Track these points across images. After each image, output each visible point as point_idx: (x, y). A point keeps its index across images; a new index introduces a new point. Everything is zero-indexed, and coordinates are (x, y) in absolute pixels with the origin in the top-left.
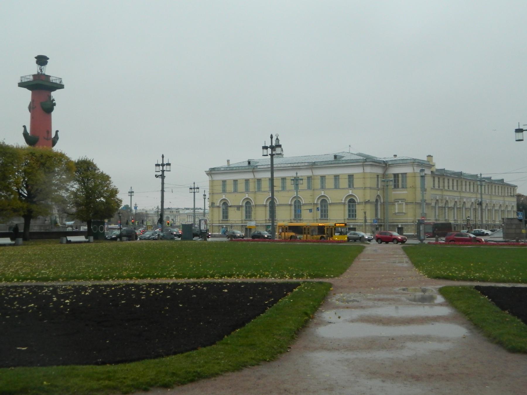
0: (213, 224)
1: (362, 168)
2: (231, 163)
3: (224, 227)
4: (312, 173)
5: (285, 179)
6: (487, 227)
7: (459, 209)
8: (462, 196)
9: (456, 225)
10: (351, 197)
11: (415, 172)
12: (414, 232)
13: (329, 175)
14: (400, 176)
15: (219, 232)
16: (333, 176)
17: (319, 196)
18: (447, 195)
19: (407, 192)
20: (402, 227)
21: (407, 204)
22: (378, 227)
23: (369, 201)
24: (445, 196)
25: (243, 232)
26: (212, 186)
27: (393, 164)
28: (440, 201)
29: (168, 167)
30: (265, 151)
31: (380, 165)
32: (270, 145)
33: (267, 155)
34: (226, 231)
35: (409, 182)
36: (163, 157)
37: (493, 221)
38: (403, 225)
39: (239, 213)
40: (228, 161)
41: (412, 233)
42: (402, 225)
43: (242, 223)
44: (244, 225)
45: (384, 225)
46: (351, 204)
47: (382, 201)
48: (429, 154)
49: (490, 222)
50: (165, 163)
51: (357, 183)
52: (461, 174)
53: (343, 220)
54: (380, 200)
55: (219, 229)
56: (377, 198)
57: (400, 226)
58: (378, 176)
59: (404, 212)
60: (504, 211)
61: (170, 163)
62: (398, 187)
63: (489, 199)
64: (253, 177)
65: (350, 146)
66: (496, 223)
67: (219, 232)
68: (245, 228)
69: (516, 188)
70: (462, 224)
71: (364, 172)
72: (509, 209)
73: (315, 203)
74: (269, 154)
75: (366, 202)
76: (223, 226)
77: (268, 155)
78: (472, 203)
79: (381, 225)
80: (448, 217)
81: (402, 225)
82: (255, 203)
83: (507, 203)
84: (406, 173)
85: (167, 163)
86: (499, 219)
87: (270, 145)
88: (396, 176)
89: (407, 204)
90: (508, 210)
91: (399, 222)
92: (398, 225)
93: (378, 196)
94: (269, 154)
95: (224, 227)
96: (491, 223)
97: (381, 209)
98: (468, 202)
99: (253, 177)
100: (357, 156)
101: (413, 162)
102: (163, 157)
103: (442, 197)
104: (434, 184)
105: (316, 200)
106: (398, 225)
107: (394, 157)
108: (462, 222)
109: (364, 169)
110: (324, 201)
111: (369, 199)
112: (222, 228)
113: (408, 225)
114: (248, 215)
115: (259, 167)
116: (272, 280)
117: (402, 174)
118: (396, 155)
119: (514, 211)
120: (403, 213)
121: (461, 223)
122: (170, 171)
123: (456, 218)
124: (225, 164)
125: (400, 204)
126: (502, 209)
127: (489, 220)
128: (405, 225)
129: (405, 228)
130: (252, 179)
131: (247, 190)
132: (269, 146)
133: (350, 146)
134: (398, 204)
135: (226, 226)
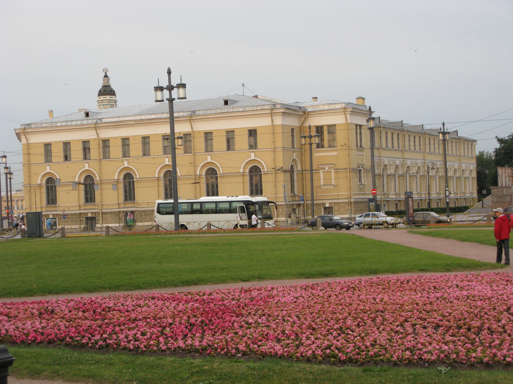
0: (102, 209)
1: (270, 118)
2: (55, 115)
3: (51, 217)
4: (192, 128)
5: (189, 136)
6: (399, 204)
7: (423, 178)
8: (405, 157)
9: (398, 200)
10: (127, 171)
11: (347, 123)
12: (349, 214)
13: (218, 131)
14: (325, 129)
15: (119, 223)
16: (225, 132)
17: (162, 165)
18: (385, 157)
19: (337, 154)
20: (331, 206)
21: (337, 172)
22: (295, 207)
23: (282, 168)
24: (383, 158)
25: (122, 222)
26: (28, 154)
27: (314, 112)
28: (400, 166)
29: (181, 90)
30: (159, 93)
31: (296, 113)
32: (168, 84)
33: (163, 101)
34: (53, 224)
35: (341, 137)
36: (169, 72)
37: (463, 193)
38: (332, 203)
39: (74, 194)
40: (51, 112)
41: (346, 214)
42: (330, 203)
43: (119, 208)
44: (84, 213)
45: (304, 204)
46: (193, 176)
47: (299, 168)
48: (360, 96)
49: (423, 196)
50: (174, 83)
51: (262, 141)
52: (401, 124)
53: (118, 205)
54: (297, 167)
55: (119, 218)
56: (292, 164)
57: (327, 205)
58: (293, 130)
59: (333, 183)
60: (460, 177)
61: (183, 82)
62: (323, 147)
63: (440, 161)
64: (96, 137)
65: (243, 85)
66: (390, 197)
67: (119, 223)
68: (85, 217)
69: (475, 143)
70: (382, 200)
71: (272, 124)
72: (467, 174)
73: (197, 175)
74: (167, 99)
75: (276, 170)
76: (48, 215)
77: (165, 99)
78: (397, 166)
79: (299, 205)
80: (388, 190)
81: (330, 203)
82: (100, 178)
83: (456, 166)
84: (334, 125)
85: (179, 82)
86: (395, 191)
87: (168, 84)
88: (319, 129)
89: (337, 172)
90: (466, 176)
91: (324, 200)
92: (325, 204)
93: (294, 160)
94: (167, 99)
95: (51, 217)
96: (461, 196)
97: (298, 181)
98: (413, 166)
99: (95, 137)
100: (236, 100)
101: (345, 108)
102: (169, 72)
103: (380, 159)
104: (293, 142)
105: (199, 168)
106: (325, 204)
107: (314, 101)
108: (383, 197)
109: (272, 120)
110: (212, 172)
111: (282, 166)
112: (47, 219)
113: (340, 203)
114: (90, 197)
115: (104, 120)
116: (438, 274)
117: (329, 126)
118: (316, 98)
119: (440, 177)
120: (332, 185)
121: (381, 199)
122: (185, 98)
123: (397, 191)
124: (45, 117)
125: (327, 172)
126: (458, 176)
127: (458, 192)
128: (335, 203)
129: (335, 208)
130: (94, 140)
131: (126, 154)
132: (165, 87)
133: (243, 85)
134: (323, 172)
135: (54, 215)
